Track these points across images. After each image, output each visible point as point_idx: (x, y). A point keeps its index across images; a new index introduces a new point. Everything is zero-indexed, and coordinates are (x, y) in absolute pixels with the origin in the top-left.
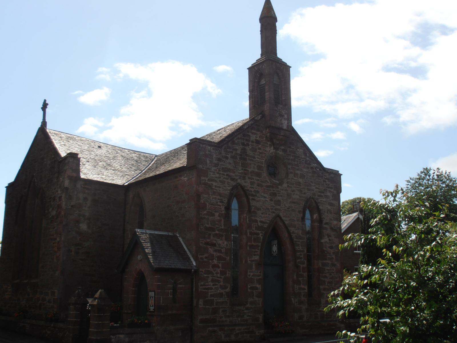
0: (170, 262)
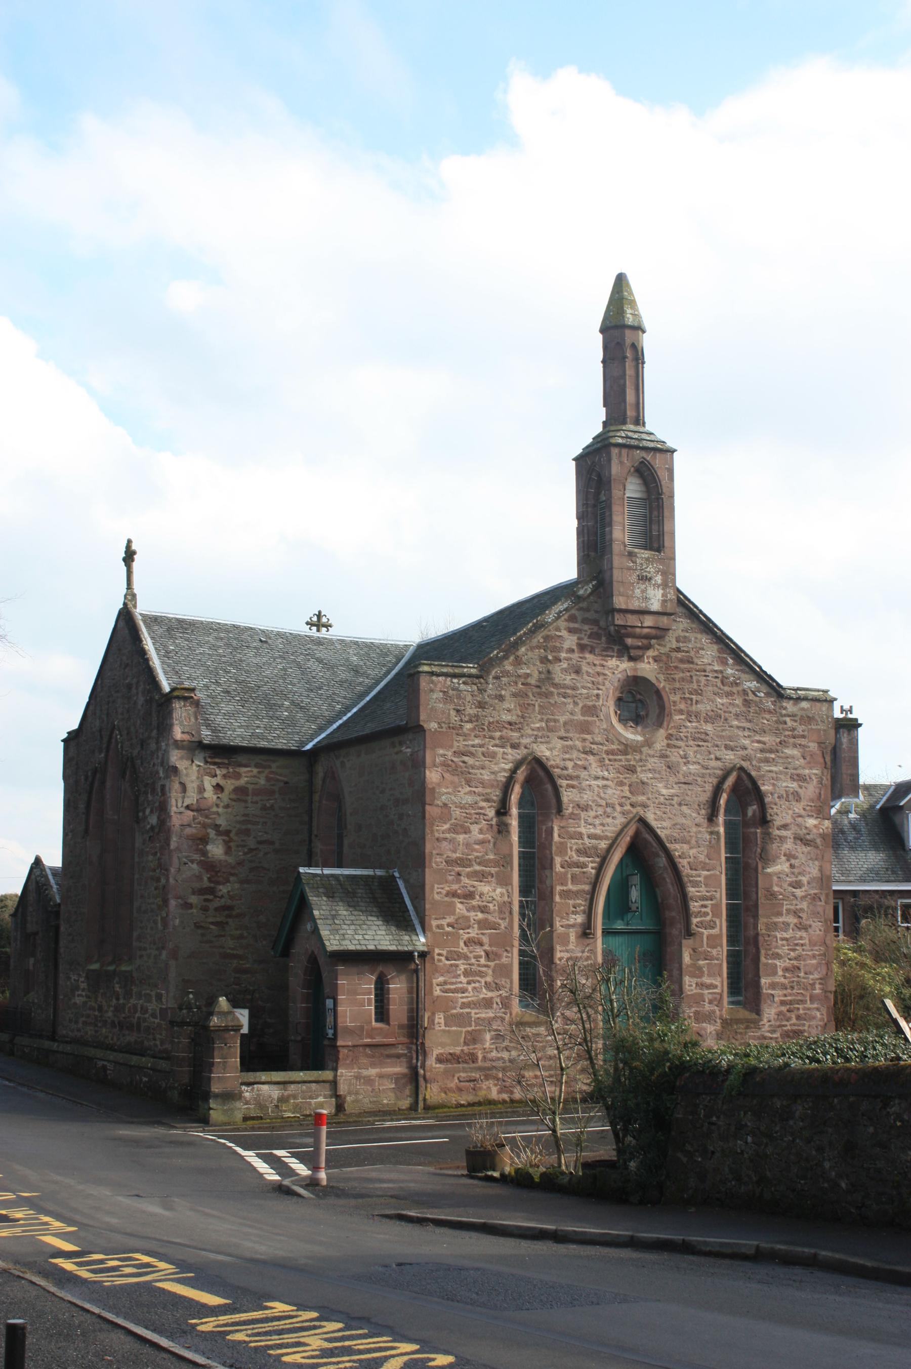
0: (366, 937)
